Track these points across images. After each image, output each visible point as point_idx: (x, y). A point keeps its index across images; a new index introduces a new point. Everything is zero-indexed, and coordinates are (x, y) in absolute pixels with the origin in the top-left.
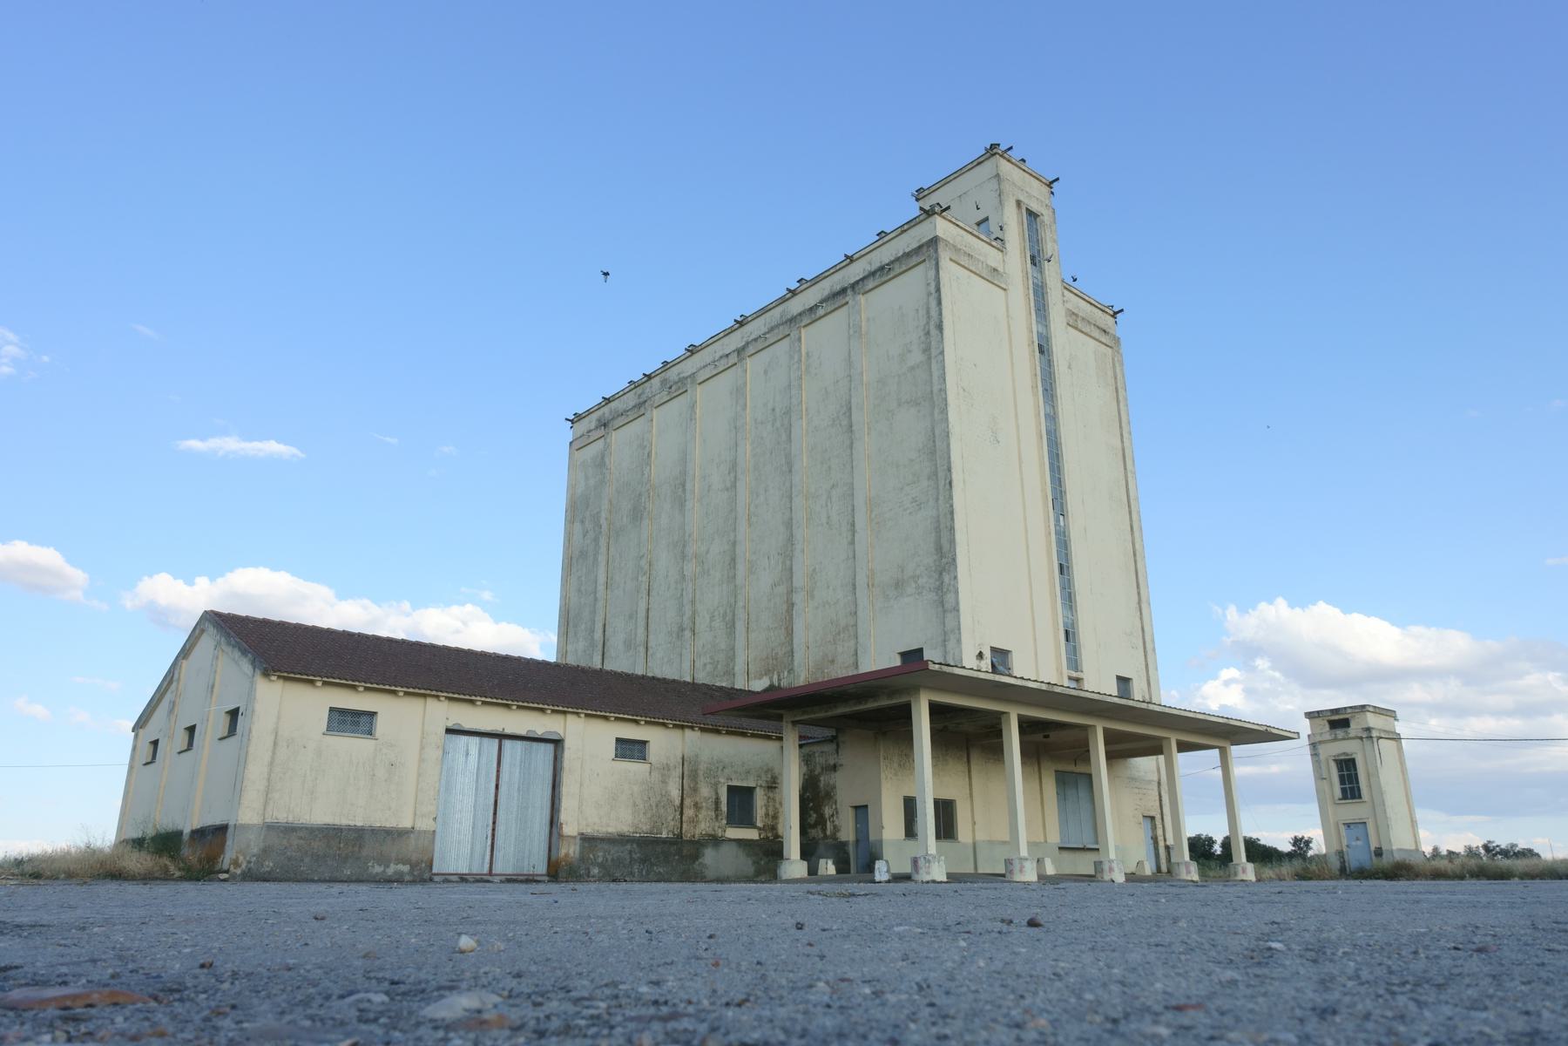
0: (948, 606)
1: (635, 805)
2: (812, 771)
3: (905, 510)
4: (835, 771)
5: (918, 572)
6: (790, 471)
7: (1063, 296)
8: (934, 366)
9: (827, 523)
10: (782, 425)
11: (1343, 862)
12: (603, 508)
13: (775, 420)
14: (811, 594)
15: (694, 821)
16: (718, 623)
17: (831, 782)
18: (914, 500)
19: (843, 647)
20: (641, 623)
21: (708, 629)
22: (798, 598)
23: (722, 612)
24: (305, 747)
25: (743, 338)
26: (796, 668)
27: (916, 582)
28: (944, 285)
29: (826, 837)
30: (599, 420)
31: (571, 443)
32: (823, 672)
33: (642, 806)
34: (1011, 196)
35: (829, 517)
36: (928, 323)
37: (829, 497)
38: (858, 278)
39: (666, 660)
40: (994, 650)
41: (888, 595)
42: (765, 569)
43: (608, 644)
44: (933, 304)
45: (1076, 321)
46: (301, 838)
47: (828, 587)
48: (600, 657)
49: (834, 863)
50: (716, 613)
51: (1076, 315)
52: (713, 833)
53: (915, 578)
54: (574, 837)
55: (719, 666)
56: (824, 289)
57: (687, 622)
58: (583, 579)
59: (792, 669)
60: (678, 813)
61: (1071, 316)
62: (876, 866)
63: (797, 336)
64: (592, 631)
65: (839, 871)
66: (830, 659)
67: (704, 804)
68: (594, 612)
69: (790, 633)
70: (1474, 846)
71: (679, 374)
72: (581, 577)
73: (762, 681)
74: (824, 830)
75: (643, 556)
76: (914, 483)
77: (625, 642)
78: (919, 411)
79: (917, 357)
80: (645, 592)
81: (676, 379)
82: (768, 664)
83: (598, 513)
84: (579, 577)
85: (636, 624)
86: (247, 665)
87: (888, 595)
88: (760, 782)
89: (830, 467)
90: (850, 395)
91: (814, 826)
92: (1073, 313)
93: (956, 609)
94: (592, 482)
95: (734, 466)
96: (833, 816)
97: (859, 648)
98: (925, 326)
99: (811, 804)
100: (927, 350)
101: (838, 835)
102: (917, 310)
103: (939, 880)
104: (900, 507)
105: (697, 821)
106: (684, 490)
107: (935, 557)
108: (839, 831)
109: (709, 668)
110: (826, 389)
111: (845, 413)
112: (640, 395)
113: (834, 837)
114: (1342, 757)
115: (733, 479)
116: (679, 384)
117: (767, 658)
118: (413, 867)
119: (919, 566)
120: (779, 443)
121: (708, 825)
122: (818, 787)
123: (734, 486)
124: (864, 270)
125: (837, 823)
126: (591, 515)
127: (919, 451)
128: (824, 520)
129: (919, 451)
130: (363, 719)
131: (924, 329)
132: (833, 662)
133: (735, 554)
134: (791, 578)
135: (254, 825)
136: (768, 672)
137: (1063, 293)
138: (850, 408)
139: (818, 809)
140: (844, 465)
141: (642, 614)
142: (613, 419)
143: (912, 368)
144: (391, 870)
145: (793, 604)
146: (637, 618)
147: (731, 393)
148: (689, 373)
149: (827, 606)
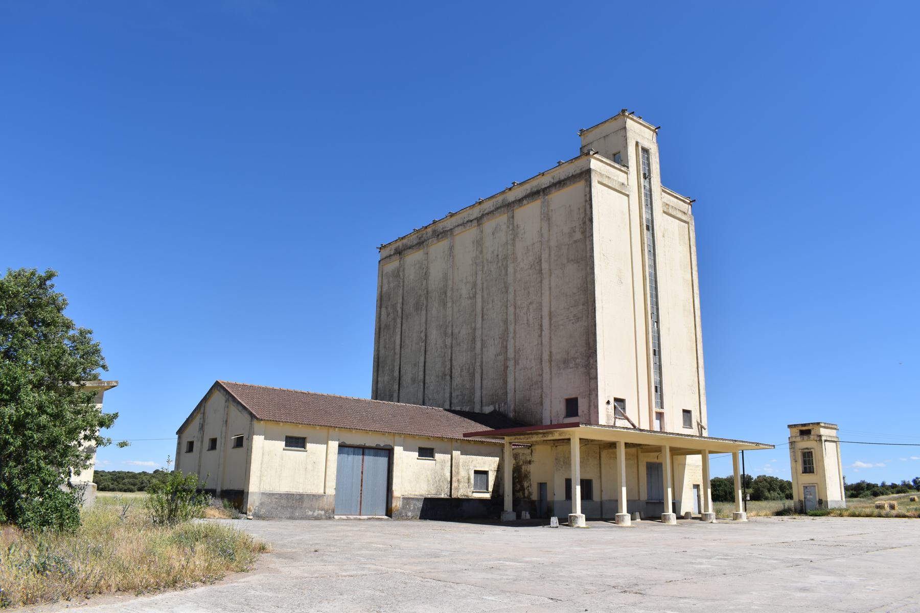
0: (592, 376)
1: (428, 480)
2: (517, 463)
3: (570, 321)
4: (530, 464)
5: (576, 356)
6: (507, 292)
7: (661, 195)
8: (588, 243)
9: (527, 323)
10: (502, 265)
11: (802, 507)
12: (399, 301)
13: (498, 262)
14: (516, 363)
15: (458, 489)
16: (465, 373)
17: (528, 470)
18: (575, 316)
19: (535, 393)
20: (421, 369)
21: (459, 376)
22: (511, 364)
23: (467, 367)
24: (276, 455)
25: (480, 212)
26: (508, 402)
27: (575, 361)
28: (594, 196)
29: (524, 497)
30: (396, 250)
31: (379, 261)
32: (523, 406)
33: (431, 481)
34: (633, 139)
35: (528, 320)
36: (585, 217)
37: (528, 309)
38: (546, 186)
39: (435, 391)
40: (616, 400)
41: (560, 367)
42: (491, 346)
43: (402, 379)
44: (588, 207)
45: (668, 209)
46: (276, 499)
47: (527, 359)
48: (397, 386)
49: (529, 513)
50: (464, 368)
51: (669, 205)
52: (467, 494)
53: (574, 359)
54: (399, 498)
55: (466, 398)
56: (527, 190)
57: (447, 371)
58: (387, 340)
59: (507, 402)
60: (449, 485)
61: (665, 206)
62: (551, 520)
63: (511, 215)
64: (393, 371)
65: (531, 517)
66: (528, 398)
67: (462, 480)
68: (393, 360)
69: (505, 382)
70: (907, 481)
71: (443, 228)
72: (386, 339)
73: (490, 408)
74: (524, 493)
75: (422, 331)
76: (575, 306)
77: (412, 379)
78: (579, 266)
79: (578, 236)
80: (423, 352)
81: (442, 231)
82: (493, 398)
83: (395, 304)
84: (385, 340)
85: (418, 369)
86: (247, 415)
87: (560, 367)
88: (490, 468)
89: (529, 292)
90: (541, 253)
91: (518, 491)
92: (667, 204)
93: (596, 378)
94: (392, 285)
95: (475, 285)
96: (528, 486)
97: (543, 394)
98: (583, 219)
99: (517, 480)
100: (583, 232)
101: (531, 497)
102: (579, 209)
103: (582, 526)
104: (567, 318)
105: (459, 489)
106: (446, 296)
107: (585, 348)
108: (531, 495)
109: (460, 397)
110: (527, 247)
111: (538, 263)
112: (420, 238)
113: (529, 497)
114: (806, 451)
115: (474, 293)
116: (443, 234)
117: (492, 395)
118: (326, 512)
119: (577, 352)
120: (500, 275)
121: (464, 490)
122: (521, 471)
123: (475, 297)
124: (550, 182)
125: (530, 490)
126: (391, 304)
127: (579, 288)
128: (525, 322)
129: (579, 288)
130: (300, 441)
131: (583, 220)
132: (529, 400)
133: (475, 335)
134: (507, 352)
135: (256, 492)
136: (493, 403)
137: (661, 193)
138: (541, 260)
139: (521, 482)
140: (537, 292)
141: (422, 364)
142: (404, 250)
143: (575, 242)
144: (316, 514)
145: (507, 367)
146: (419, 366)
147: (473, 243)
148: (449, 229)
149: (526, 370)
